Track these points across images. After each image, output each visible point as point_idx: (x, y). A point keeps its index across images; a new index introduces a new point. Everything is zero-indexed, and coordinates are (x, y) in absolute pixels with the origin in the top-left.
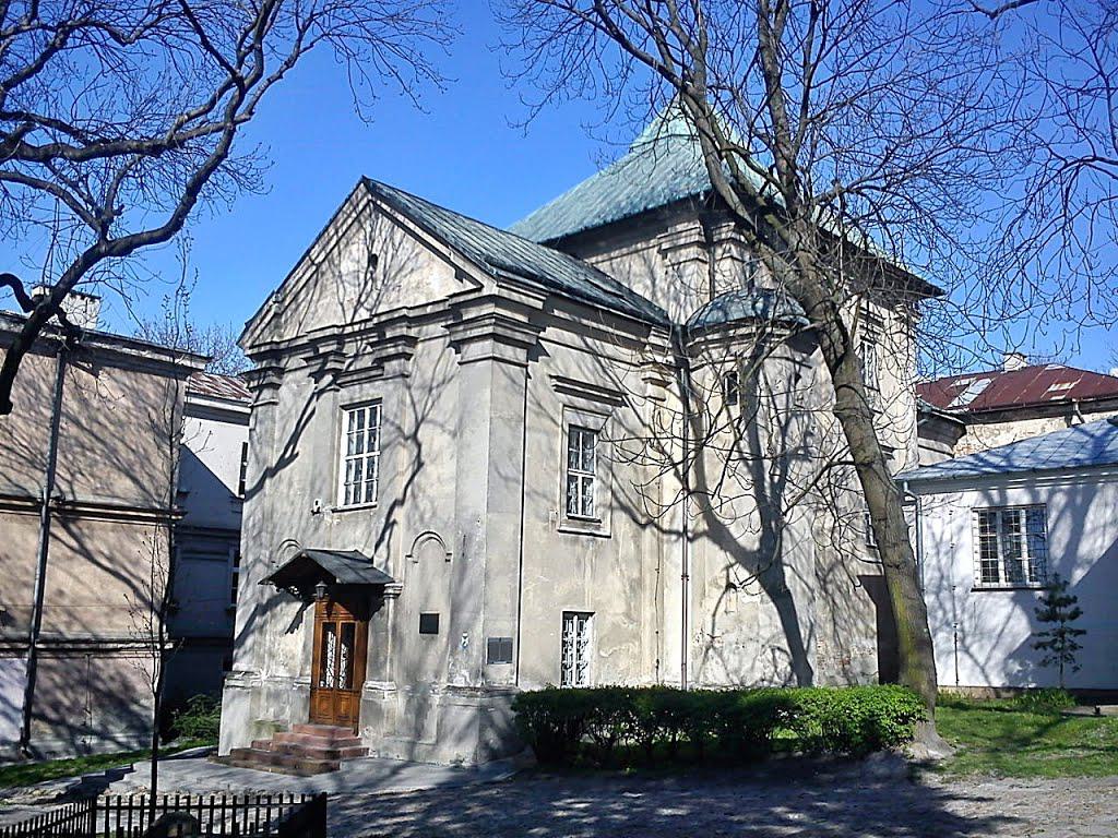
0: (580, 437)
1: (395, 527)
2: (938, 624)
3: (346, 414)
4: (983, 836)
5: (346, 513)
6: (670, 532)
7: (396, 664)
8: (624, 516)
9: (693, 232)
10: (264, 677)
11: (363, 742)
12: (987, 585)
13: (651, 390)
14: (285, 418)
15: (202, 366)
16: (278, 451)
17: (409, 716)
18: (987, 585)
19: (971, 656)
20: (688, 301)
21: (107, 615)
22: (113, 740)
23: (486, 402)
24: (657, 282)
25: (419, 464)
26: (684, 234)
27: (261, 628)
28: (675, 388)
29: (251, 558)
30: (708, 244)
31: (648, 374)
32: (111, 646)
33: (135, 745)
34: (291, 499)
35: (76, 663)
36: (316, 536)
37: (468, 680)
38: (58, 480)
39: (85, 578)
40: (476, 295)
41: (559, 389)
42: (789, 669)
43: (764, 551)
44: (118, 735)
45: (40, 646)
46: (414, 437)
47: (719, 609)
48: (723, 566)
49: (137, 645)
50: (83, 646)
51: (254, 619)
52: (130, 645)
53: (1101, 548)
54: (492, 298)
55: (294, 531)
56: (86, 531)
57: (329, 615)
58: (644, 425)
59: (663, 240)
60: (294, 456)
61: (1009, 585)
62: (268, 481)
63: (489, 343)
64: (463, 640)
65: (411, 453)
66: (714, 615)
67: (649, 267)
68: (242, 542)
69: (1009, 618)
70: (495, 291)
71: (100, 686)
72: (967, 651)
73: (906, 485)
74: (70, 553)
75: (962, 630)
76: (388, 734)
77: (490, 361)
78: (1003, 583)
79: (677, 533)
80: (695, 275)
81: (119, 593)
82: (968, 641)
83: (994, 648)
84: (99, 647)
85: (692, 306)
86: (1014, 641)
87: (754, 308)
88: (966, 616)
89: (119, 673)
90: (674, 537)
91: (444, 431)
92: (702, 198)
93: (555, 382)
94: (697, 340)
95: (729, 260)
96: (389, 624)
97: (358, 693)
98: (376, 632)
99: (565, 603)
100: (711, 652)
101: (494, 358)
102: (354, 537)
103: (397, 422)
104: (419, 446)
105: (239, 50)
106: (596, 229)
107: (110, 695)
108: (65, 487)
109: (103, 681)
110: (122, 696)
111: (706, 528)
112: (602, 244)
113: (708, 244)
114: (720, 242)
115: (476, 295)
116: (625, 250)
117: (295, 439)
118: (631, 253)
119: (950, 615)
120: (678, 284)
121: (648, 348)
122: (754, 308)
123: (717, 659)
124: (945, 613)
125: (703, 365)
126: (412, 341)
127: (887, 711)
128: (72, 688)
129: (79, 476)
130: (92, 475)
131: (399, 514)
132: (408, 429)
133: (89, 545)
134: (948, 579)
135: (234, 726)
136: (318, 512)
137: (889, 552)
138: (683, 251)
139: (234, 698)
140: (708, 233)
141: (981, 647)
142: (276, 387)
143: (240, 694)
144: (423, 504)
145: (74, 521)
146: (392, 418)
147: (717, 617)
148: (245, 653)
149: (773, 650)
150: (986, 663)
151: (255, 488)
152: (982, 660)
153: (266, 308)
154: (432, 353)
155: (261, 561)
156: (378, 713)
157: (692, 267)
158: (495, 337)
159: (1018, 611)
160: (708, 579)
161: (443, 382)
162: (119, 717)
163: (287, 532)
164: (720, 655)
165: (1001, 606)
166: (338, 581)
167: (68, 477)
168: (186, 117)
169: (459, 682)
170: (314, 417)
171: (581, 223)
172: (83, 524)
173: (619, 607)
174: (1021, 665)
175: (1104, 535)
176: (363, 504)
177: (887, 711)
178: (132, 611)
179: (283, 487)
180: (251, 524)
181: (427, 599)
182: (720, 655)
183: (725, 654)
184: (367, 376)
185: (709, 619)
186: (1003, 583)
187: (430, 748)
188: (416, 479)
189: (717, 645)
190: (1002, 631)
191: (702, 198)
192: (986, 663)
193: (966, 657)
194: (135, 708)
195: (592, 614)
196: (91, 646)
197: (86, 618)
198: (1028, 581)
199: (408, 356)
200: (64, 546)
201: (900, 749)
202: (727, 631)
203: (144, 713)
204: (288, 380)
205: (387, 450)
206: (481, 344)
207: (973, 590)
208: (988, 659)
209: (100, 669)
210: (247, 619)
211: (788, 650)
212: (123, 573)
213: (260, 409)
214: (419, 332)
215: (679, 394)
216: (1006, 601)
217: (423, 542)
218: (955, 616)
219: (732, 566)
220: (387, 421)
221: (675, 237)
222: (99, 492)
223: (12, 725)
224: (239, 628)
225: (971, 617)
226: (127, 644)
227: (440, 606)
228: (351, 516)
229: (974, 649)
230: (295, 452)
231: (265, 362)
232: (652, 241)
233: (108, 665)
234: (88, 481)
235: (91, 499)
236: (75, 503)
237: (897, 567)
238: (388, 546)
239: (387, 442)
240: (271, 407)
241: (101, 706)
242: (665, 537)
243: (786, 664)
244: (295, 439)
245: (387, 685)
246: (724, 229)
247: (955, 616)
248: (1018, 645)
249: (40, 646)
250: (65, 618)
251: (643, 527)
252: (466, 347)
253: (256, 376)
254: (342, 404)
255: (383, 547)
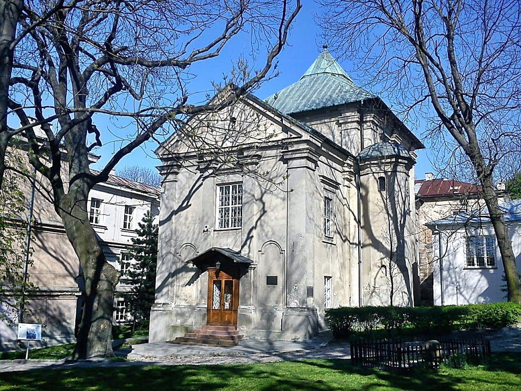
0: (328, 200)
1: (253, 238)
2: (448, 283)
3: (218, 188)
4: (296, 390)
5: (222, 232)
6: (353, 244)
7: (254, 298)
8: (338, 235)
9: (355, 116)
10: (173, 305)
11: (239, 333)
12: (469, 267)
13: (347, 183)
14: (182, 189)
15: (95, 160)
16: (178, 203)
17: (263, 321)
18: (469, 267)
19: (463, 296)
20: (352, 146)
21: (53, 279)
22: (55, 339)
23: (303, 186)
24: (335, 137)
25: (264, 212)
26: (351, 117)
27: (172, 284)
28: (353, 182)
29: (164, 252)
30: (361, 122)
31: (346, 176)
32: (56, 294)
33: (65, 341)
34: (188, 225)
35: (40, 302)
36: (206, 242)
37: (298, 304)
38: (34, 213)
39: (45, 261)
40: (299, 139)
41: (323, 181)
42: (408, 300)
43: (398, 252)
44: (57, 337)
45: (26, 294)
46: (261, 200)
47: (378, 276)
48: (379, 258)
49: (67, 293)
50: (44, 294)
51: (169, 279)
52: (64, 293)
53: (517, 253)
54: (307, 141)
55: (190, 239)
56: (45, 238)
57: (217, 277)
58: (344, 198)
59: (340, 119)
60: (187, 206)
61: (478, 267)
62: (174, 216)
63: (304, 161)
64: (295, 287)
65: (259, 207)
66: (375, 279)
67: (331, 130)
68: (158, 244)
69: (479, 280)
70: (309, 138)
71: (50, 313)
72: (461, 294)
73: (436, 226)
74: (38, 249)
75: (459, 286)
76: (253, 329)
77: (305, 168)
78: (476, 266)
79: (356, 244)
80: (355, 135)
81: (60, 269)
82: (462, 290)
83: (473, 292)
84: (50, 294)
85: (354, 148)
86: (481, 290)
87: (395, 151)
88: (461, 280)
89: (58, 307)
90: (354, 246)
91: (278, 198)
92: (362, 103)
93: (321, 178)
94: (366, 163)
95: (370, 130)
96: (252, 281)
97: (236, 311)
98: (244, 286)
99: (325, 272)
100: (374, 294)
101: (307, 167)
102: (228, 242)
103: (252, 193)
104: (264, 204)
105: (227, 25)
106: (307, 111)
107: (53, 317)
108: (36, 216)
109: (52, 311)
110: (59, 318)
111: (371, 242)
112: (308, 118)
113: (361, 122)
114: (366, 122)
115: (299, 139)
116: (319, 122)
117: (188, 198)
118: (322, 123)
119: (454, 280)
120: (347, 138)
121: (346, 165)
122: (395, 151)
123: (377, 296)
124: (452, 278)
125: (368, 174)
126: (259, 157)
127: (512, 311)
128: (38, 314)
129: (42, 211)
130: (48, 211)
131: (254, 233)
132: (257, 194)
133: (46, 245)
134: (453, 265)
135: (158, 329)
136: (207, 231)
137: (506, 251)
138: (349, 124)
139: (157, 316)
140: (361, 118)
141: (467, 293)
142: (177, 173)
143: (161, 314)
144: (267, 229)
145: (40, 233)
146: (249, 191)
147: (377, 279)
148: (162, 296)
149: (402, 293)
150: (469, 299)
151: (166, 219)
152: (468, 297)
153: (172, 137)
154: (270, 164)
155: (171, 253)
156: (248, 321)
157: (353, 132)
158: (308, 158)
159: (483, 278)
160: (372, 263)
161: (276, 176)
162: (58, 328)
163: (185, 240)
164: (378, 295)
165: (476, 276)
166: (235, 261)
167: (38, 211)
168: (197, 52)
169: (293, 305)
170: (202, 186)
171: (297, 108)
172: (46, 235)
173: (338, 275)
174: (484, 299)
175: (518, 248)
176: (230, 228)
177: (512, 311)
178: (64, 276)
179: (182, 220)
180: (163, 236)
181: (269, 270)
182: (378, 295)
183: (381, 295)
184: (231, 171)
185: (373, 280)
186: (476, 266)
187: (280, 334)
188: (262, 218)
189: (376, 291)
190: (476, 286)
191: (362, 103)
192: (469, 299)
193: (461, 296)
194: (64, 323)
195: (331, 277)
196: (48, 293)
197: (45, 280)
198: (487, 266)
199: (257, 164)
200: (36, 245)
201: (514, 326)
202: (382, 285)
203: (68, 326)
204: (182, 171)
205: (247, 205)
206: (299, 160)
207: (464, 269)
208: (470, 297)
209: (50, 305)
210: (163, 280)
211: (408, 293)
212: (60, 259)
213: (167, 183)
214: (262, 153)
215: (355, 185)
216: (478, 274)
217: (267, 245)
218: (456, 280)
219: (383, 258)
220: (246, 192)
221: (346, 118)
222: (51, 219)
223: (13, 332)
224: (158, 284)
225: (463, 280)
226: (62, 293)
227: (276, 272)
228: (224, 233)
229: (464, 293)
230: (189, 204)
231: (169, 162)
232: (333, 119)
233: (53, 303)
234: (47, 214)
235: (48, 223)
236: (41, 224)
237: (509, 257)
238: (249, 247)
239: (246, 201)
240: (175, 183)
241: (51, 323)
242: (351, 246)
243: (407, 298)
244: (188, 198)
245: (252, 307)
246: (368, 117)
247: (456, 280)
248: (483, 291)
249: (26, 294)
250: (36, 280)
251: (344, 241)
252: (291, 161)
253: (166, 168)
254: (217, 183)
255: (246, 247)
